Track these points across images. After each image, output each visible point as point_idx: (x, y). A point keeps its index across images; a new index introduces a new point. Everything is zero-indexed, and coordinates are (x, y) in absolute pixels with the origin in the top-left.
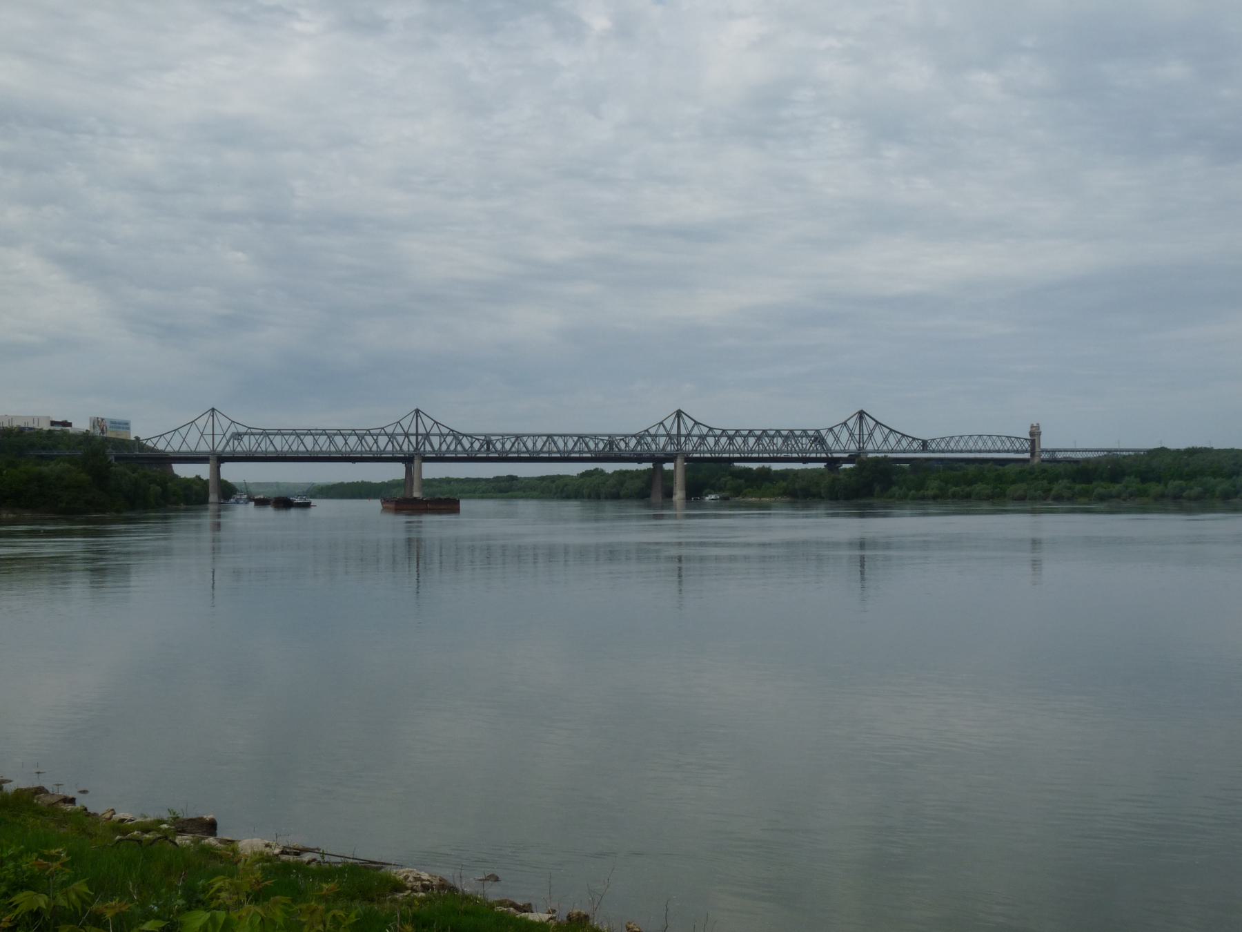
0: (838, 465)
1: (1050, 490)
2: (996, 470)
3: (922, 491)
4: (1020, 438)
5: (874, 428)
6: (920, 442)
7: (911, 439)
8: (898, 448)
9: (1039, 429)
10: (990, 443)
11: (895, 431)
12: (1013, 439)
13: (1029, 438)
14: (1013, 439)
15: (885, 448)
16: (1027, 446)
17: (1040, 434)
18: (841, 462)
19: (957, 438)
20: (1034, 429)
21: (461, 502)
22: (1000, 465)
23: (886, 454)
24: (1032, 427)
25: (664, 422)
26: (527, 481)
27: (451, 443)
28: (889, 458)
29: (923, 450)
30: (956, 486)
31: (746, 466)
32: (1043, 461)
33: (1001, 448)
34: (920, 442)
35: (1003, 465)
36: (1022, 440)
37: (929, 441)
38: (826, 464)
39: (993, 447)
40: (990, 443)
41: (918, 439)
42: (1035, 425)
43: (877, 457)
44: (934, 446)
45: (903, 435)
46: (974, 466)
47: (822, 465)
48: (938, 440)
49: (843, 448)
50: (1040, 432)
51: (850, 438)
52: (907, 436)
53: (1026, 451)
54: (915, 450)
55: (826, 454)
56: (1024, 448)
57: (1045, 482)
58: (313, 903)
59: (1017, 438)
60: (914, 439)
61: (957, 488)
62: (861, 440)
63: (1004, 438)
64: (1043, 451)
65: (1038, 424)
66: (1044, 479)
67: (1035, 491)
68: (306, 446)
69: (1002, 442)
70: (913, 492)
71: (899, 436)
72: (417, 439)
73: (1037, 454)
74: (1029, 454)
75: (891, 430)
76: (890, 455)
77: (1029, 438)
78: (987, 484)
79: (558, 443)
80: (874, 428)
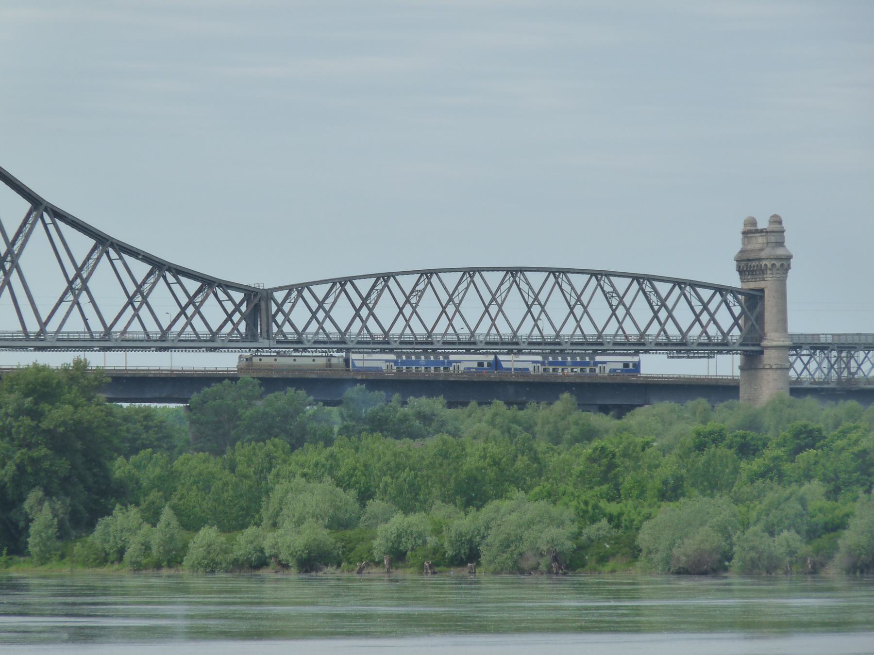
1: (836, 527)
2: (588, 434)
3: (251, 531)
4: (694, 285)
5: (25, 230)
6: (238, 296)
7: (193, 286)
8: (136, 327)
9: (781, 244)
10: (684, 315)
11: (57, 214)
12: (663, 288)
13: (734, 281)
14: (663, 288)
15: (75, 325)
16: (725, 319)
17: (784, 264)
19: (408, 282)
20: (759, 241)
21: (765, 351)
22: (604, 409)
23: (81, 355)
24: (750, 231)
26: (45, 373)
27: (369, 295)
30: (407, 510)
32: (798, 391)
33: (525, 330)
34: (238, 296)
35: (621, 411)
36: (706, 294)
37: (279, 296)
39: (571, 323)
40: (684, 315)
41: (227, 286)
42: (763, 224)
43: (39, 369)
44: (300, 316)
45: (159, 266)
46: (488, 412)
47: (591, 351)
48: (321, 291)
49: (97, 327)
50: (789, 258)
53: (723, 346)
54: (214, 335)
56: (712, 330)
57: (815, 489)
59: (679, 283)
60: (208, 283)
61: (414, 518)
63: (621, 284)
64: (796, 346)
65: (777, 220)
66: (809, 477)
67: (771, 532)
68: (677, 307)
69: (616, 300)
70: (208, 534)
71: (141, 269)
73: (770, 357)
74: (737, 360)
75: (103, 241)
76: (96, 360)
77: (734, 281)
78: (552, 496)
80: (25, 230)
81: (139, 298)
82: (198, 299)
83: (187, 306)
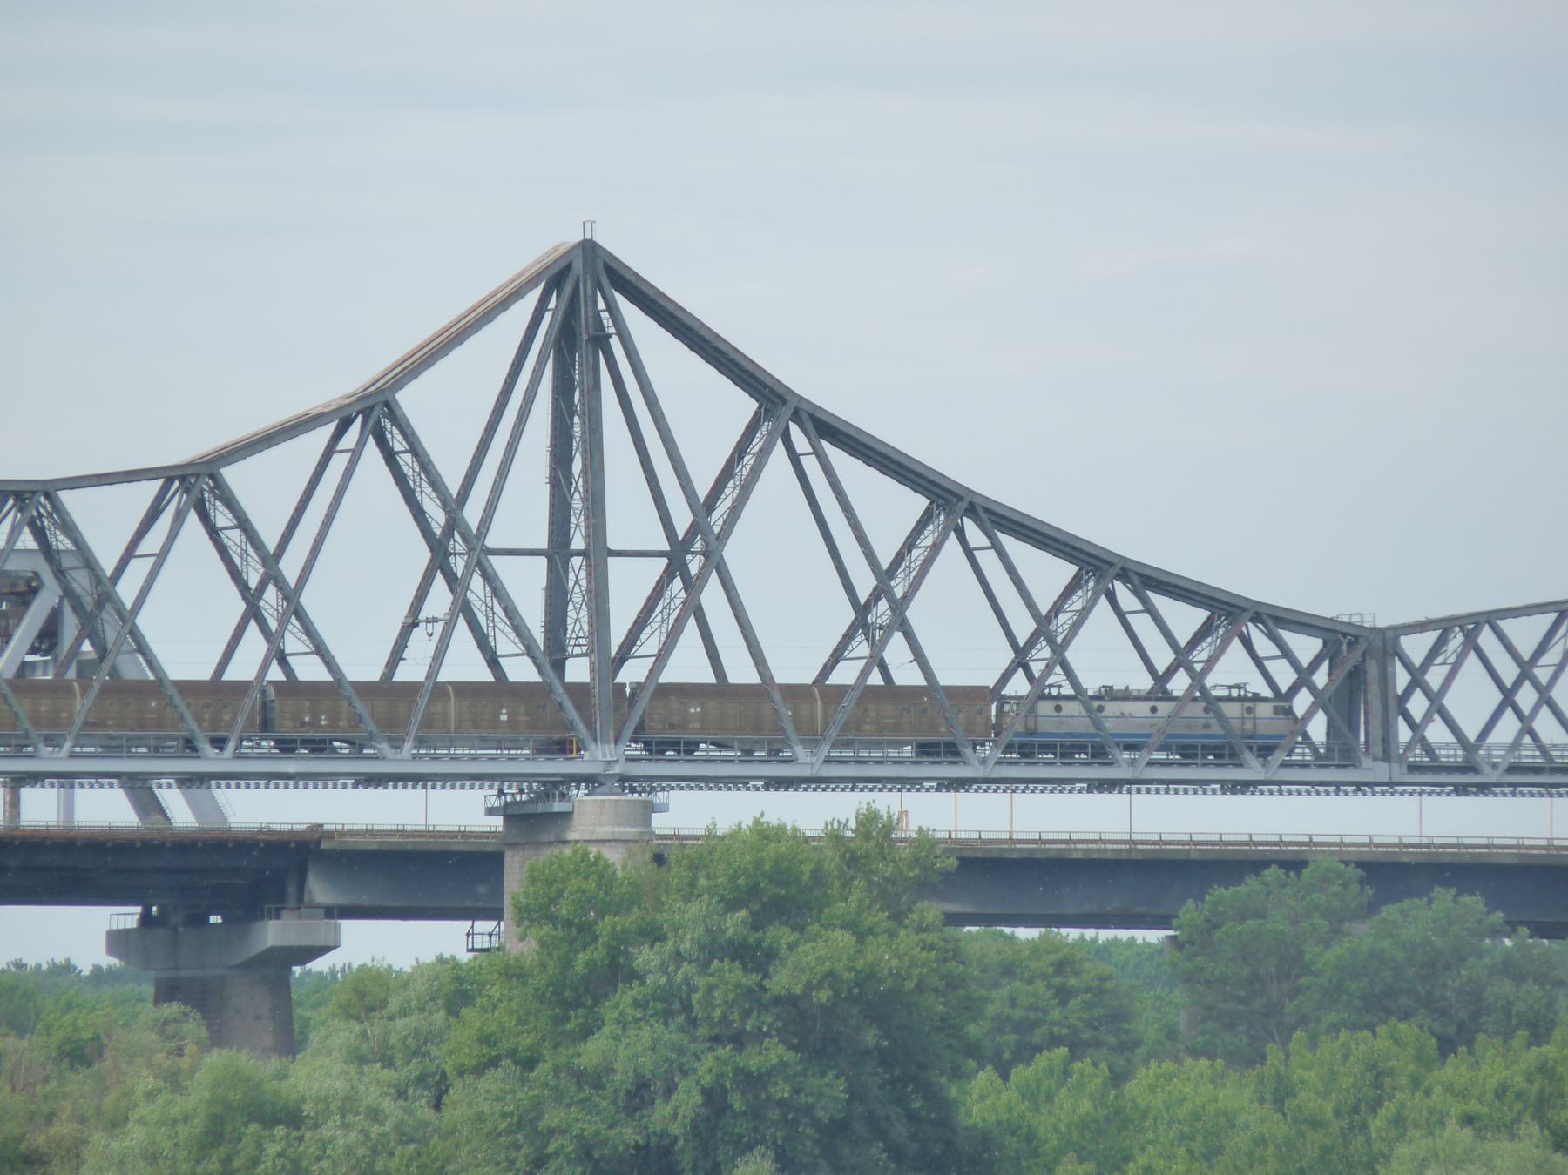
0: (274, 933)
6: (1306, 647)
11: (826, 429)
18: (320, 890)
25: (408, 399)
28: (925, 842)
29: (1340, 751)
31: (772, 819)
34: (1306, 647)
37: (1416, 647)
38: (127, 916)
41: (1276, 620)
43: (765, 834)
46: (1396, 907)
51: (440, 599)
52: (1148, 581)
55: (139, 788)
58: (1180, 1152)
62: (578, 620)
72: (1295, 664)
79: (842, 664)
81: (1043, 652)
82: (1201, 654)
83: (1171, 671)
